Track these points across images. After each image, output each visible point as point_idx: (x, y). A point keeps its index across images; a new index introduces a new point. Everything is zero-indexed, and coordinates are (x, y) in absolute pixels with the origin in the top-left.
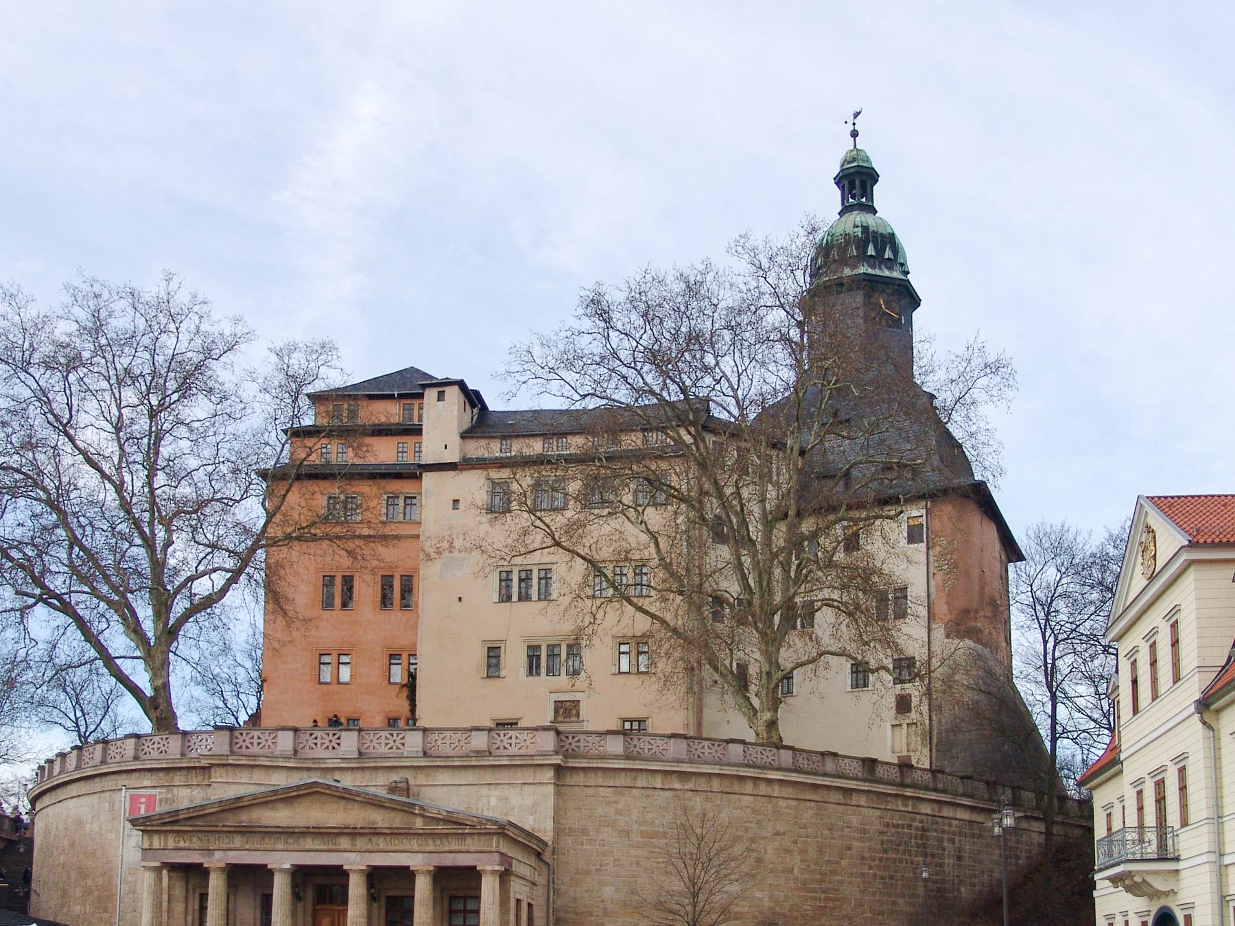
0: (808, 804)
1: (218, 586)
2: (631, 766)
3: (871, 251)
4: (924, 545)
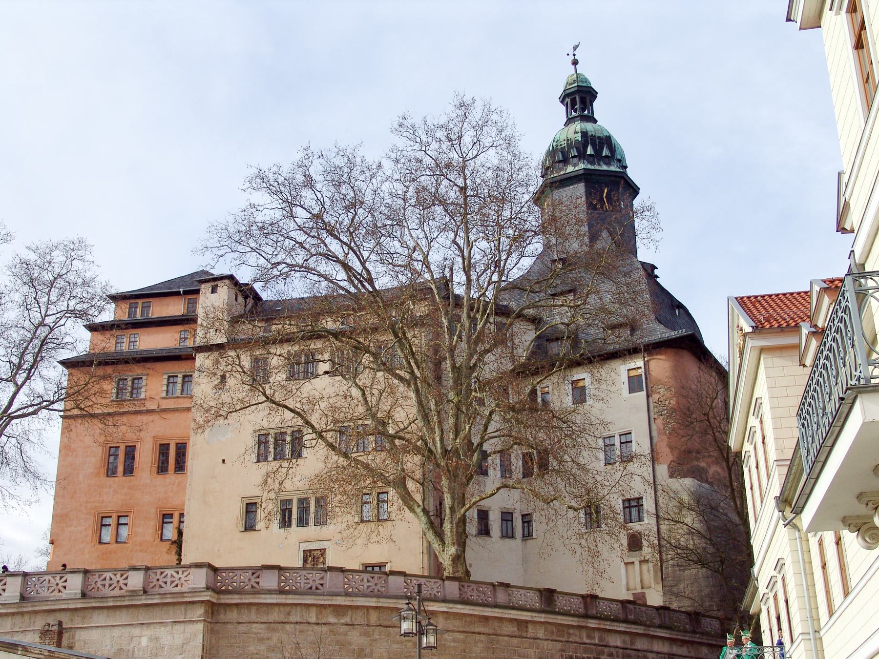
0: (478, 637)
2: (283, 601)
3: (590, 150)
4: (644, 393)
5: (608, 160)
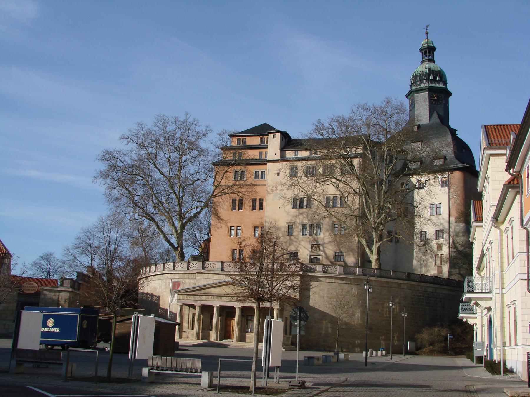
1: (199, 211)
3: (431, 77)
5: (439, 82)
